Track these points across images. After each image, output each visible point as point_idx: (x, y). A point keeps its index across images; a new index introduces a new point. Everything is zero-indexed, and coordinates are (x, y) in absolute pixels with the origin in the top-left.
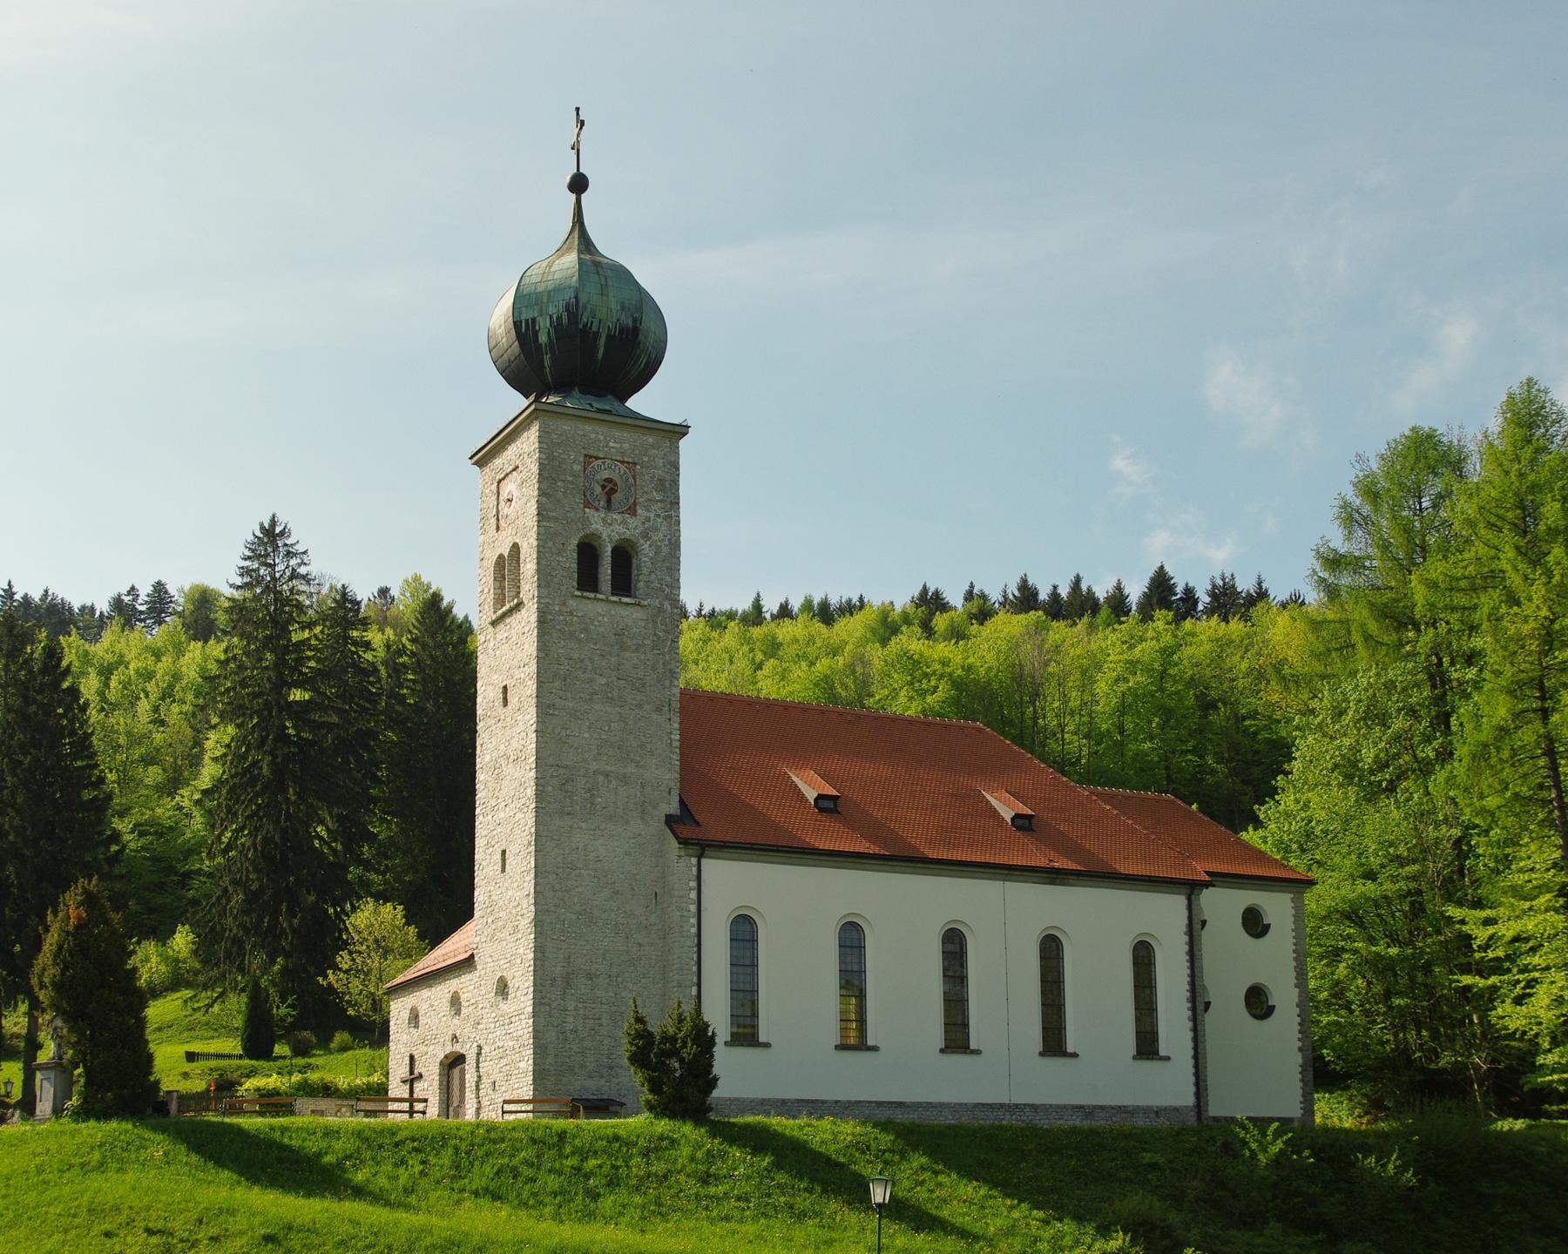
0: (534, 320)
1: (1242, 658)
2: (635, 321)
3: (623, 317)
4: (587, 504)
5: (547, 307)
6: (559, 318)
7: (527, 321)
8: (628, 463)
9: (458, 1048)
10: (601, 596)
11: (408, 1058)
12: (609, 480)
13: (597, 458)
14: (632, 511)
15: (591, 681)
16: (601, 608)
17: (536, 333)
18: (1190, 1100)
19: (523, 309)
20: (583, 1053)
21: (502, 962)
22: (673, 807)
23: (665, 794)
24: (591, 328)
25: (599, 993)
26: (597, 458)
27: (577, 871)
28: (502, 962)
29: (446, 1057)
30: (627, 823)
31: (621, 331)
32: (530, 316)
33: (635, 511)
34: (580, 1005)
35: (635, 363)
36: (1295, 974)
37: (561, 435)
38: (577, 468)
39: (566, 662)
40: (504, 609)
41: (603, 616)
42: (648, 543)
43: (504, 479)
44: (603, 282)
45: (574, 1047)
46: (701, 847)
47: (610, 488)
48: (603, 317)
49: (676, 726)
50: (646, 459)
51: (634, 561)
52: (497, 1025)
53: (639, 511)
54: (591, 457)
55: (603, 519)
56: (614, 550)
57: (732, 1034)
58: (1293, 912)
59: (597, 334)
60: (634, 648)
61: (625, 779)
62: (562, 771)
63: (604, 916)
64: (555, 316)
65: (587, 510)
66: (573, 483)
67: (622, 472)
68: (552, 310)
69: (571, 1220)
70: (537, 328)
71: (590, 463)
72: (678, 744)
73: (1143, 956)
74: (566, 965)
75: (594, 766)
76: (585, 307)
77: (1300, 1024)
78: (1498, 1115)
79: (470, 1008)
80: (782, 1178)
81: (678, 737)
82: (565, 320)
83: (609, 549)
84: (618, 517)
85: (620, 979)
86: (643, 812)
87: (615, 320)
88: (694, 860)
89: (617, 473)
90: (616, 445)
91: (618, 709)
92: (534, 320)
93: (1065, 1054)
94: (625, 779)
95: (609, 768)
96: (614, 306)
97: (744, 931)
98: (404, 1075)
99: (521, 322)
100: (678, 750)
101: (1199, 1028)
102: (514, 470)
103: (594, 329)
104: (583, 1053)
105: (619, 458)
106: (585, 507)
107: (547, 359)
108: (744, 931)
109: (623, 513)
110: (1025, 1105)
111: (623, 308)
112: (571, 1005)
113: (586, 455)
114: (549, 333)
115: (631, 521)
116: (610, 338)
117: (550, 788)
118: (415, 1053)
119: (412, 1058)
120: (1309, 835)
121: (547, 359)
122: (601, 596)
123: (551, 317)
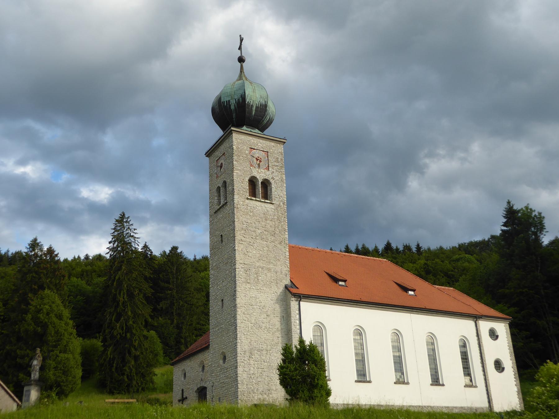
0: (229, 101)
2: (265, 102)
3: (261, 100)
4: (251, 165)
5: (234, 96)
6: (239, 100)
7: (227, 101)
8: (265, 152)
9: (203, 384)
10: (257, 199)
11: (181, 391)
13: (254, 149)
14: (268, 168)
16: (258, 204)
17: (230, 106)
18: (487, 405)
19: (225, 97)
20: (257, 383)
21: (222, 346)
22: (288, 282)
23: (284, 276)
24: (250, 103)
25: (263, 358)
26: (254, 149)
27: (253, 306)
28: (222, 346)
29: (198, 389)
30: (271, 287)
31: (261, 105)
32: (228, 99)
33: (269, 169)
34: (256, 363)
35: (266, 117)
36: (509, 355)
37: (241, 140)
38: (247, 152)
39: (245, 224)
40: (220, 206)
41: (259, 207)
42: (274, 181)
43: (219, 159)
44: (254, 88)
45: (254, 381)
46: (300, 297)
49: (288, 250)
50: (272, 150)
51: (269, 188)
52: (221, 372)
53: (270, 169)
54: (252, 149)
55: (258, 171)
56: (261, 183)
58: (505, 331)
59: (252, 106)
60: (270, 219)
62: (246, 266)
64: (237, 99)
65: (251, 168)
66: (246, 157)
67: (263, 154)
68: (236, 97)
69: (287, 331)
70: (230, 104)
71: (251, 151)
72: (288, 257)
73: (464, 345)
74: (250, 345)
75: (258, 264)
76: (248, 96)
77: (514, 375)
78: (517, 413)
79: (209, 367)
81: (288, 254)
82: (241, 100)
83: (260, 182)
85: (271, 352)
87: (258, 101)
88: (297, 303)
90: (260, 145)
91: (266, 243)
92: (229, 101)
93: (440, 385)
94: (269, 270)
95: (263, 265)
98: (179, 399)
99: (224, 102)
100: (288, 259)
101: (486, 374)
102: (223, 155)
103: (251, 104)
104: (257, 383)
105: (262, 150)
106: (251, 166)
107: (234, 115)
109: (264, 169)
110: (428, 406)
111: (261, 97)
112: (252, 362)
113: (250, 148)
114: (235, 105)
115: (268, 173)
116: (257, 107)
117: (241, 272)
118: (184, 389)
119: (183, 390)
120: (313, 404)
121: (234, 115)
122: (257, 199)
123: (235, 99)
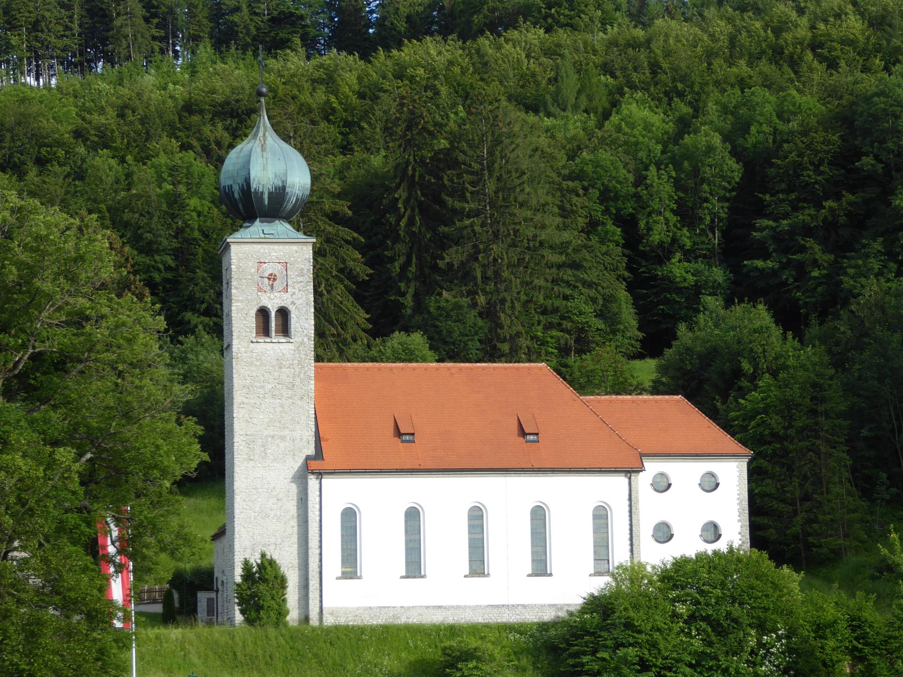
1: (820, 546)
2: (283, 182)
12: (271, 275)
14: (286, 290)
15: (262, 387)
17: (233, 193)
31: (276, 189)
47: (272, 278)
48: (265, 183)
57: (343, 573)
59: (262, 193)
61: (283, 438)
63: (273, 513)
73: (601, 516)
75: (266, 433)
80: (846, 475)
84: (278, 295)
86: (294, 455)
89: (276, 269)
94: (283, 438)
96: (271, 176)
97: (349, 517)
107: (240, 205)
108: (349, 517)
111: (276, 176)
116: (270, 194)
121: (240, 205)
